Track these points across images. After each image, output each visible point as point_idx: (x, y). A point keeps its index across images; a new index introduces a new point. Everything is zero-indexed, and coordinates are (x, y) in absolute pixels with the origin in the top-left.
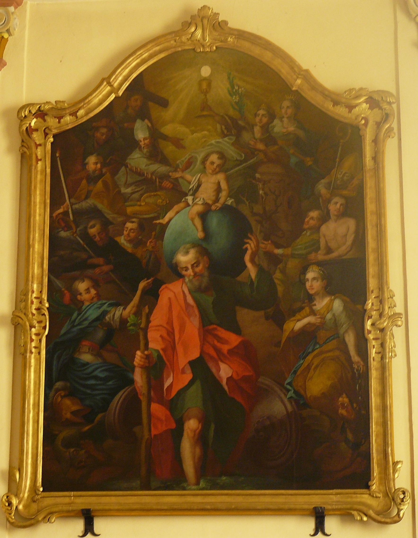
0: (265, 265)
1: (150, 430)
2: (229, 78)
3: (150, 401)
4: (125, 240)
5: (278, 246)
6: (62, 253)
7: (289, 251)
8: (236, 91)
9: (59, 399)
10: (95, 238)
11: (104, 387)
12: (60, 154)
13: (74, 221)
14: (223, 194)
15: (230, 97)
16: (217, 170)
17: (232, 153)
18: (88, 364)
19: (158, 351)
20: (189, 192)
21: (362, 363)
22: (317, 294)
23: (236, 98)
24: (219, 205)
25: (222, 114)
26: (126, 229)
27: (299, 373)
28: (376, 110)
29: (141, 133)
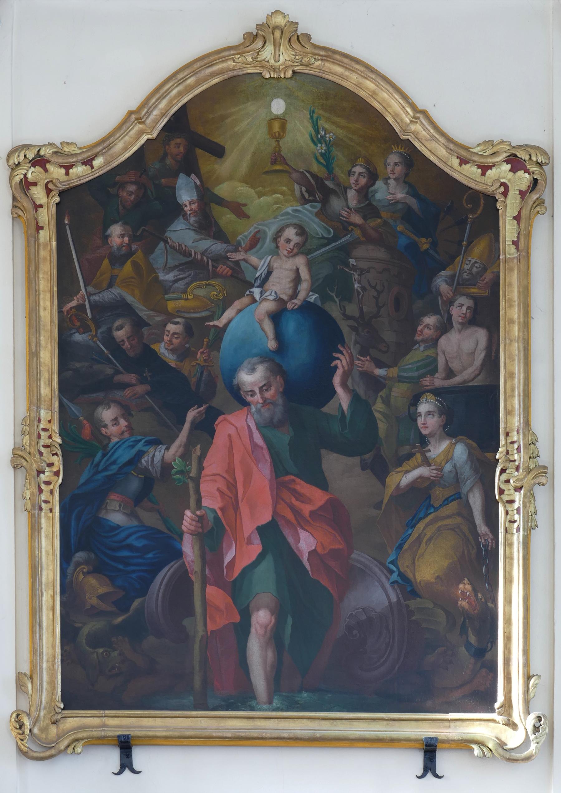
0: (361, 391)
1: (205, 625)
2: (312, 118)
3: (204, 582)
4: (166, 349)
5: (380, 364)
6: (78, 365)
7: (393, 372)
8: (322, 137)
9: (81, 576)
10: (123, 345)
11: (140, 561)
12: (70, 220)
13: (94, 319)
14: (304, 287)
15: (312, 146)
16: (295, 250)
17: (316, 227)
18: (119, 527)
19: (214, 511)
20: (255, 282)
21: (490, 535)
22: (432, 435)
23: (321, 148)
24: (298, 301)
25: (301, 170)
26: (167, 333)
27: (405, 547)
28: (521, 173)
29: (186, 195)
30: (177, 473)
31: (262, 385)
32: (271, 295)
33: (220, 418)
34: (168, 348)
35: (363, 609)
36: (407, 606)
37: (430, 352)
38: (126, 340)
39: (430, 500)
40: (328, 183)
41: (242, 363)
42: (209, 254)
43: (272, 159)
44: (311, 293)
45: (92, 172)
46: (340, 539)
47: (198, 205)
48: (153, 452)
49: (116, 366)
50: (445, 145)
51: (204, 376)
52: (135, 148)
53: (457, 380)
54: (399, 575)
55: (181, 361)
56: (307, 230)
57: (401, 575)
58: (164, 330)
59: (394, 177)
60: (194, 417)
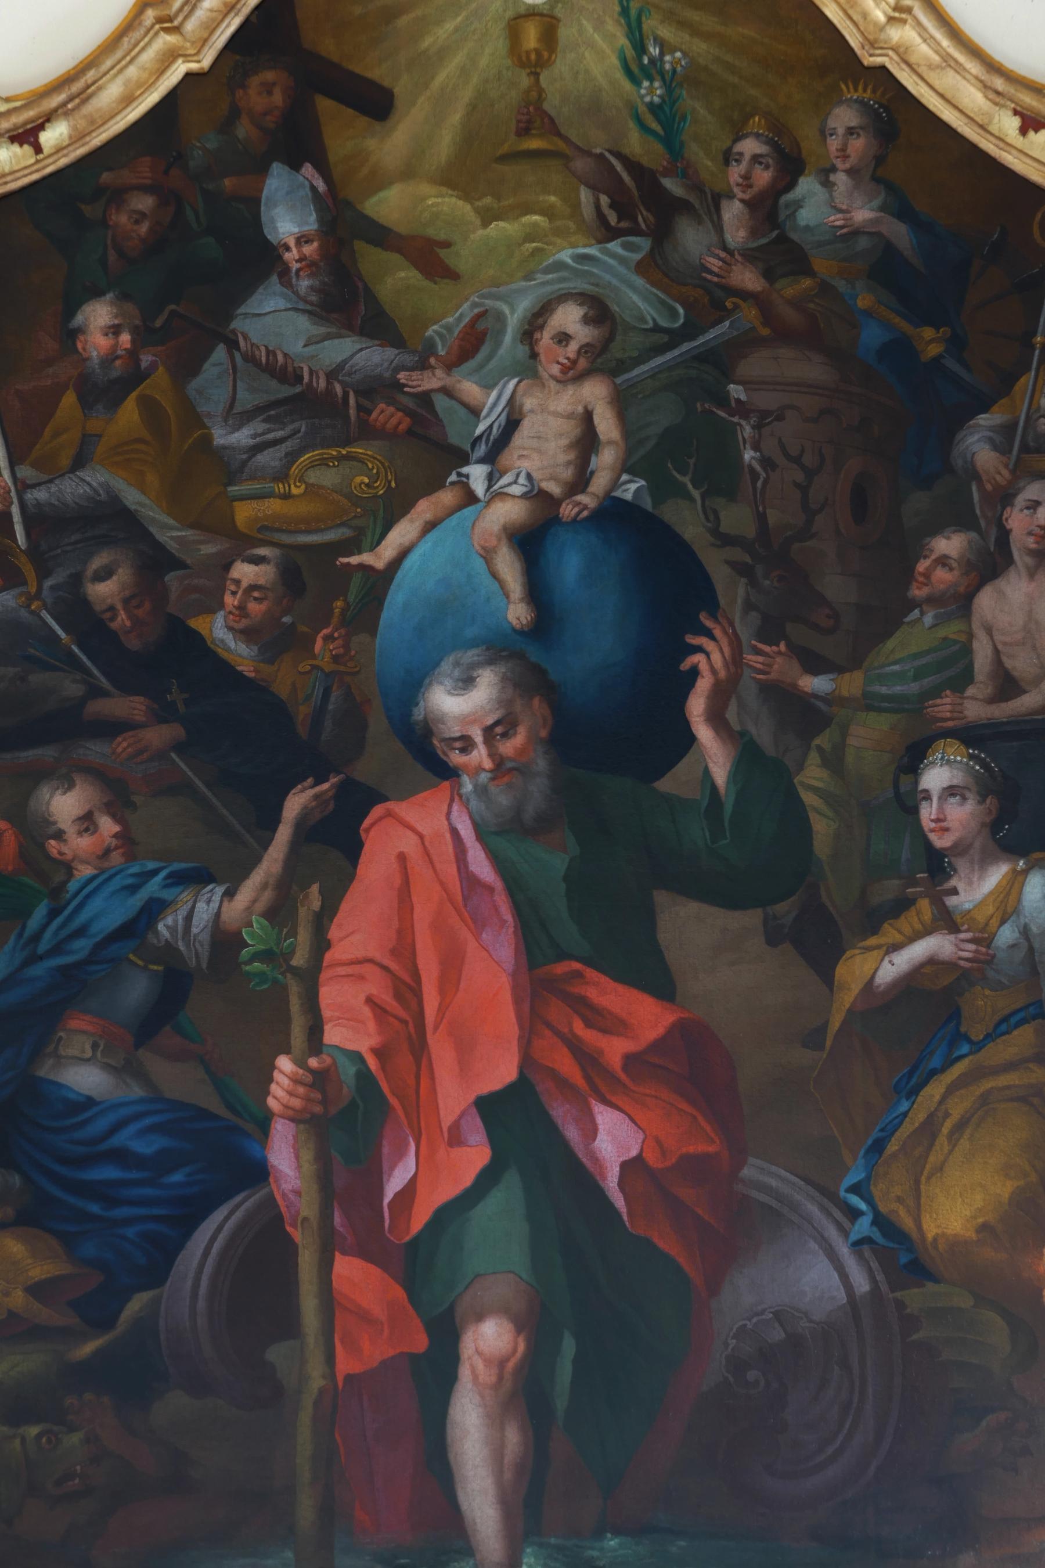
0: (764, 735)
1: (330, 1359)
2: (625, 11)
3: (329, 1246)
4: (230, 629)
5: (814, 664)
7: (852, 684)
8: (652, 61)
10: (113, 619)
13: (34, 552)
14: (606, 459)
15: (627, 85)
16: (583, 363)
17: (638, 301)
18: (90, 1102)
19: (357, 1057)
20: (473, 450)
22: (960, 849)
23: (651, 90)
25: (598, 151)
26: (233, 588)
27: (893, 1147)
30: (255, 957)
31: (490, 721)
32: (515, 482)
33: (377, 811)
34: (236, 626)
35: (777, 1315)
36: (900, 1305)
37: (952, 630)
38: (119, 606)
39: (959, 1024)
40: (672, 185)
41: (437, 664)
42: (350, 374)
43: (519, 122)
44: (625, 477)
45: (38, 161)
46: (708, 1129)
47: (321, 247)
48: (190, 904)
49: (89, 673)
50: (981, 81)
51: (332, 699)
52: (153, 98)
53: (1027, 702)
54: (874, 1223)
55: (271, 662)
56: (615, 308)
57: (880, 1221)
58: (224, 579)
59: (847, 166)
60: (305, 807)
